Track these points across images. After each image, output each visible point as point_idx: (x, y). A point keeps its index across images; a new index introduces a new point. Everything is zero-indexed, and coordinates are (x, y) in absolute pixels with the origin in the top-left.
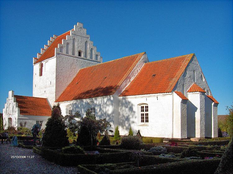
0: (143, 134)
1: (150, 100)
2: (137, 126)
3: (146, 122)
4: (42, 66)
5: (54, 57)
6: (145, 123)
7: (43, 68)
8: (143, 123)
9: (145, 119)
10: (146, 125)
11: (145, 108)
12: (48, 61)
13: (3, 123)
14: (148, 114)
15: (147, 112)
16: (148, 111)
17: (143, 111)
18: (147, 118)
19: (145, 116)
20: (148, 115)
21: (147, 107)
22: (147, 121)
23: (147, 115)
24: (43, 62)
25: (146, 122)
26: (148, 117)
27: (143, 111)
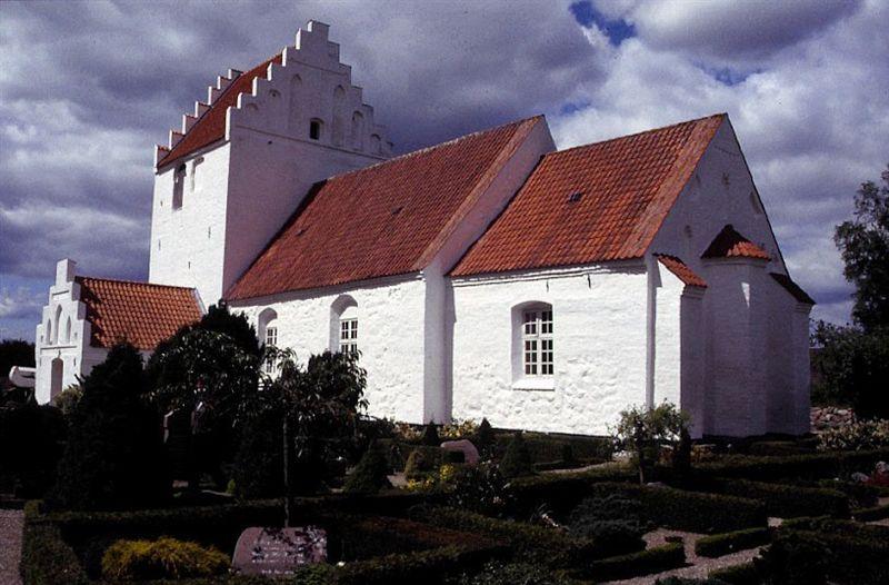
9: (539, 359)
11: (535, 314)
14: (551, 342)
15: (547, 336)
17: (544, 343)
18: (548, 357)
23: (548, 344)
26: (551, 354)
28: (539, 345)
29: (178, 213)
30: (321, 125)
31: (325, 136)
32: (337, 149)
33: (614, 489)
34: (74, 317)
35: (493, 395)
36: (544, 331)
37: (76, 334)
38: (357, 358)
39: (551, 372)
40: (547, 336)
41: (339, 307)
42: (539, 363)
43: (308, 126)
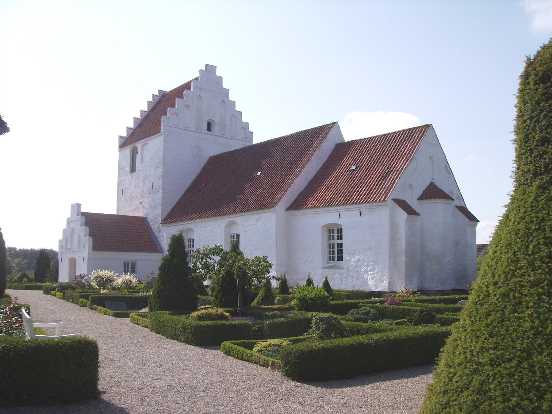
0: (335, 285)
1: (346, 217)
2: (156, 276)
3: (338, 260)
4: (134, 153)
5: (160, 134)
6: (336, 263)
7: (138, 156)
8: (332, 263)
9: (335, 253)
10: (340, 267)
11: (335, 233)
12: (147, 142)
13: (16, 288)
14: (342, 244)
15: (340, 241)
16: (342, 239)
17: (338, 244)
18: (340, 252)
19: (336, 249)
20: (342, 247)
21: (340, 231)
22: (340, 258)
23: (340, 246)
24: (139, 145)
25: (338, 260)
26: (342, 250)
27: (338, 244)
28: (336, 246)
29: (135, 174)
30: (213, 123)
31: (216, 129)
32: (223, 136)
33: (365, 306)
34: (83, 235)
35: (311, 268)
36: (338, 239)
37: (84, 244)
38: (271, 267)
39: (342, 260)
40: (340, 241)
41: (231, 224)
42: (336, 255)
43: (206, 125)
